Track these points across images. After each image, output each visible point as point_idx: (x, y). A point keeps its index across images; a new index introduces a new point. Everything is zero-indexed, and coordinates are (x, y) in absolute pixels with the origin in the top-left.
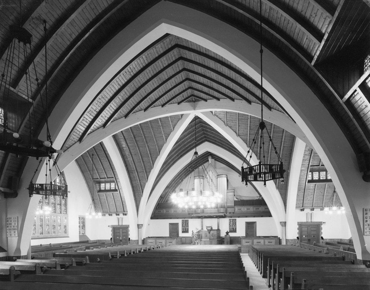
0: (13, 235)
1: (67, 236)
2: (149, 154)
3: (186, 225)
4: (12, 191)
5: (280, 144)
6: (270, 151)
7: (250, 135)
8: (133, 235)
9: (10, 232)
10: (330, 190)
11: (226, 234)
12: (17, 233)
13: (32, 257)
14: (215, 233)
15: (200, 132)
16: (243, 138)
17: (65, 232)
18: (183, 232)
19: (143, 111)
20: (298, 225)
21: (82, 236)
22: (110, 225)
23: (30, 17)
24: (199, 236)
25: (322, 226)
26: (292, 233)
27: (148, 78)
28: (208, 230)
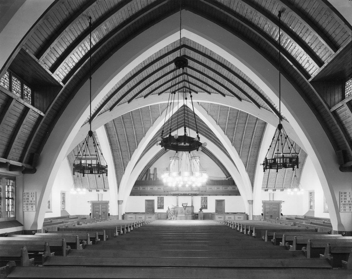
0: (30, 209)
1: (50, 211)
2: (135, 136)
3: (161, 202)
4: (32, 168)
5: (252, 134)
6: (243, 139)
7: (228, 125)
8: (113, 210)
9: (344, 207)
10: (289, 174)
11: (200, 210)
12: (35, 208)
13: (46, 231)
14: (190, 209)
15: (185, 117)
16: (222, 126)
17: (49, 208)
18: (158, 208)
19: (143, 98)
20: (262, 203)
21: (63, 211)
22: (90, 200)
23: (82, 14)
24: (175, 213)
25: (282, 204)
26: (258, 210)
27: (155, 70)
28: (184, 207)
